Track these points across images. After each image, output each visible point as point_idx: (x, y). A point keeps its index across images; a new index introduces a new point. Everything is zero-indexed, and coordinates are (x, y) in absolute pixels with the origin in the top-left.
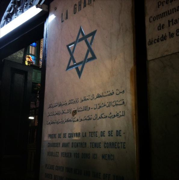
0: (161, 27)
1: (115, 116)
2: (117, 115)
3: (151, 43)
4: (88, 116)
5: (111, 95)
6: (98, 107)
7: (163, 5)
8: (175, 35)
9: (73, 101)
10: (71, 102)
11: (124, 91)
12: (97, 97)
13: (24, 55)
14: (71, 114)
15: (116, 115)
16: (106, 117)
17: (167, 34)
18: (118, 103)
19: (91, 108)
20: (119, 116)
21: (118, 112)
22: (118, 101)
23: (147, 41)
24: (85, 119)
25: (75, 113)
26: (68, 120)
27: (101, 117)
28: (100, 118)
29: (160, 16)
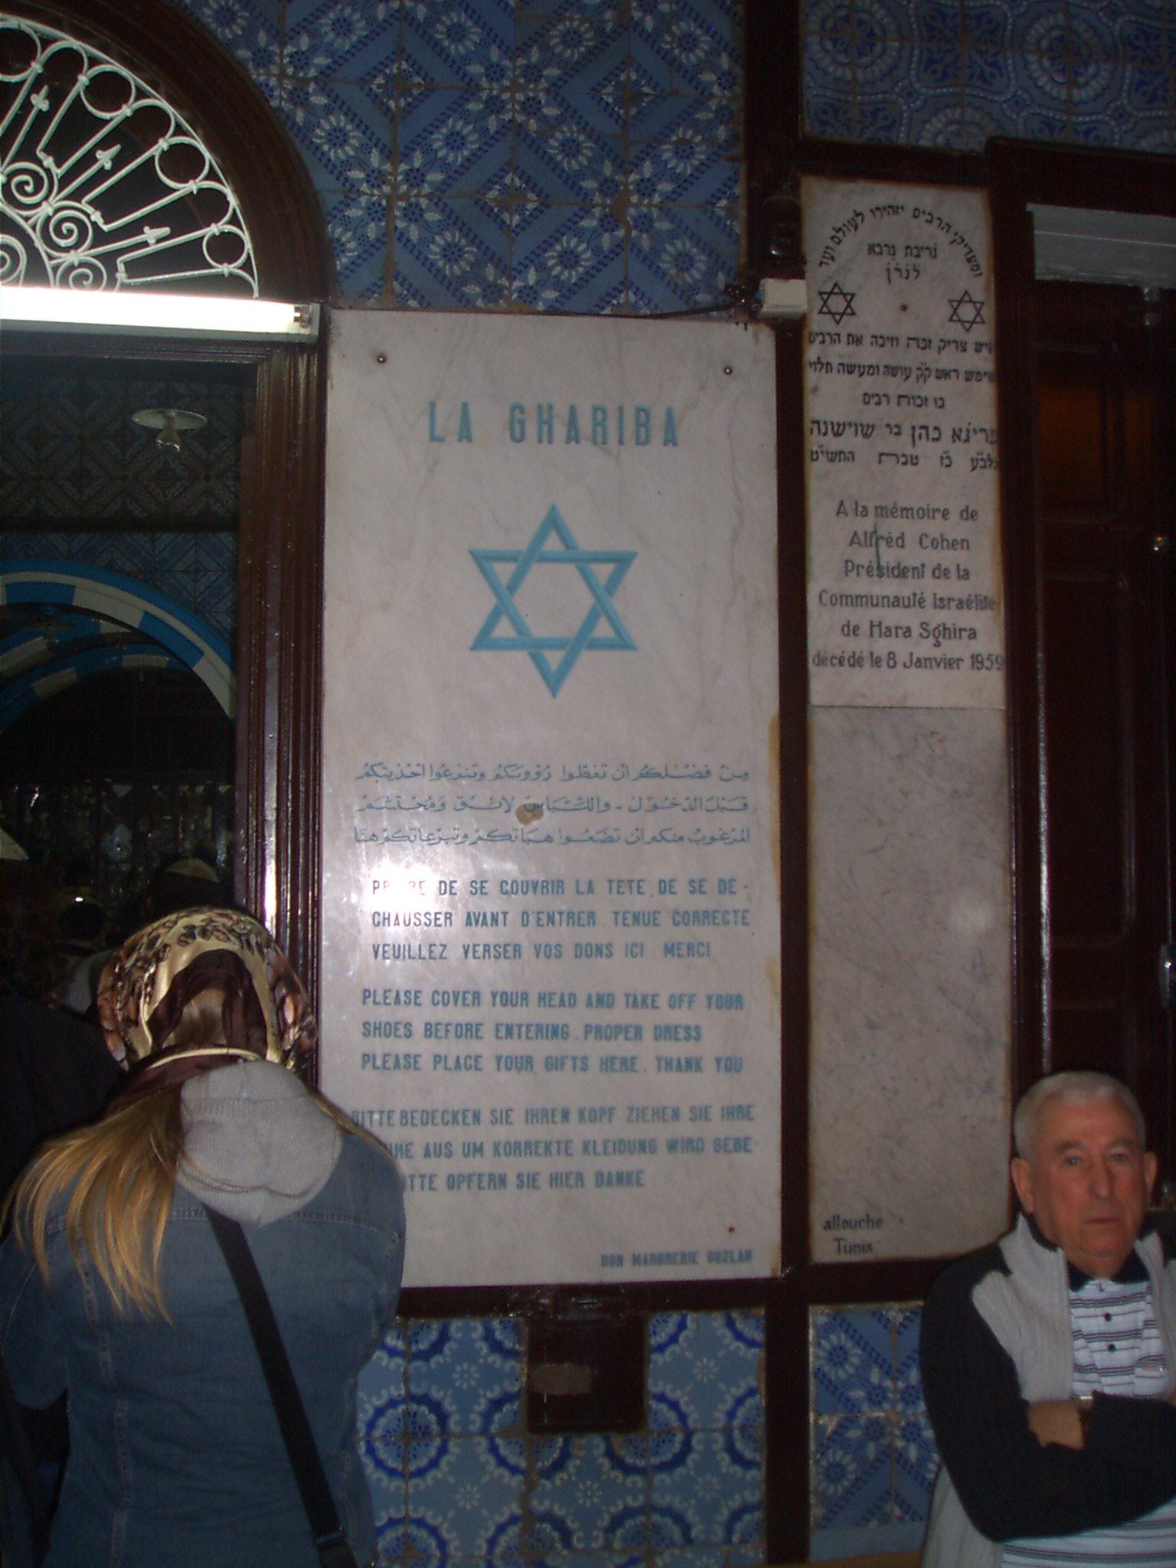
8: (884, 663)
9: (522, 771)
11: (746, 774)
12: (641, 776)
17: (866, 655)
28: (654, 839)
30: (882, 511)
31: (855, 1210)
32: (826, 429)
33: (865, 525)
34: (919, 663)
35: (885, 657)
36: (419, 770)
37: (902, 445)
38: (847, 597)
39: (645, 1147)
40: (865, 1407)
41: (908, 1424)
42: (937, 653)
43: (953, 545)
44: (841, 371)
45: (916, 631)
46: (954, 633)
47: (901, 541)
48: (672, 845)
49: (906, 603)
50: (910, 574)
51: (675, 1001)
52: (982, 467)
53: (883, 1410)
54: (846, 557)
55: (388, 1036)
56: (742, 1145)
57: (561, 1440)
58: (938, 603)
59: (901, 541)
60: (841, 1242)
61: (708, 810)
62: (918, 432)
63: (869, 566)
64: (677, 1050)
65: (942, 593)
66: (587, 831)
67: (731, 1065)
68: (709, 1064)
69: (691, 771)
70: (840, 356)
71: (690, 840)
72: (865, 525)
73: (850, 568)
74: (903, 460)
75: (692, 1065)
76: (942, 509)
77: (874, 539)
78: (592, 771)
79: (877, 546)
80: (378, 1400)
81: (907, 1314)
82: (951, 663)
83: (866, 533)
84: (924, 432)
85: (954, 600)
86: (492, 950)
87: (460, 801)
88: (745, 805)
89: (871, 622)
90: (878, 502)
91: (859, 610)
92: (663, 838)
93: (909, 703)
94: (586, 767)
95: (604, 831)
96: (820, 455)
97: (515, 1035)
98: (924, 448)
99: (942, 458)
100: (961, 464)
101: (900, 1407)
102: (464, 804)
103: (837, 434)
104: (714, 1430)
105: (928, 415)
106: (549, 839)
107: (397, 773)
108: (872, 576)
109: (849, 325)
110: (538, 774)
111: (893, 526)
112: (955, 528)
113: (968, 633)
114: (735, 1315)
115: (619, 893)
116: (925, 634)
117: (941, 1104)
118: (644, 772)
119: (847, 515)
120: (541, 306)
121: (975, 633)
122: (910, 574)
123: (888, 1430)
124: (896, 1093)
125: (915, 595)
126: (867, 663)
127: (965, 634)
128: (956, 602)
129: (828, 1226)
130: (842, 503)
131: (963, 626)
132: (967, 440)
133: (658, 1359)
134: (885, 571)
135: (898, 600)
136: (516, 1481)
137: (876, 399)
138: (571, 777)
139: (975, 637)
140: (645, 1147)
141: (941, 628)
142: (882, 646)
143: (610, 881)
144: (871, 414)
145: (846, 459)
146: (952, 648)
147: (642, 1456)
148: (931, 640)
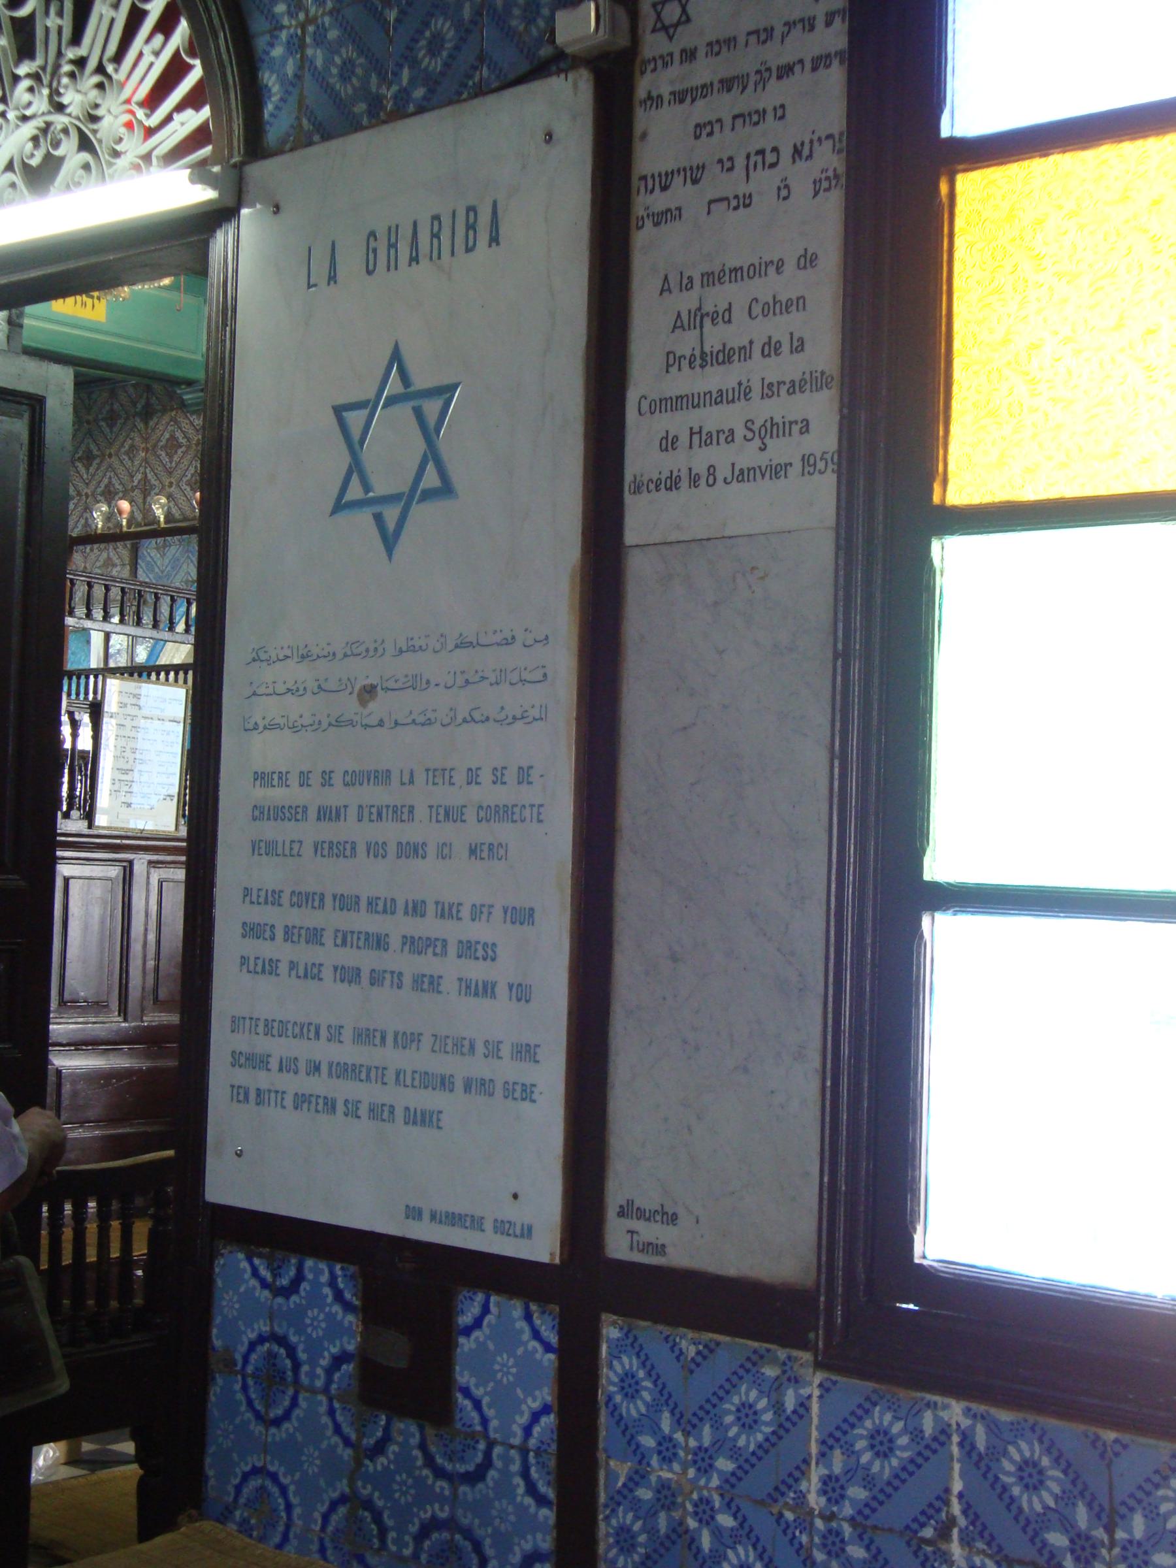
6: (460, 681)
7: (680, 369)
8: (703, 482)
9: (362, 649)
11: (547, 638)
12: (457, 646)
17: (684, 474)
22: (528, 670)
23: (628, 478)
24: (409, 720)
25: (368, 693)
28: (465, 721)
30: (710, 279)
31: (649, 1200)
32: (654, 185)
33: (686, 302)
34: (742, 475)
35: (704, 474)
36: (289, 653)
37: (734, 184)
38: (666, 399)
39: (445, 1083)
40: (655, 1461)
41: (701, 1499)
42: (762, 460)
43: (787, 307)
44: (672, 102)
45: (740, 432)
46: (773, 429)
47: (726, 315)
48: (480, 725)
49: (730, 397)
50: (736, 357)
51: (477, 912)
52: (825, 190)
53: (671, 1470)
54: (667, 350)
55: (258, 938)
56: (527, 1093)
57: (384, 1417)
58: (766, 391)
59: (726, 315)
60: (635, 1236)
61: (511, 684)
62: (753, 159)
63: (693, 355)
64: (477, 971)
65: (772, 378)
66: (411, 713)
67: (521, 993)
68: (502, 990)
69: (498, 638)
70: (672, 82)
71: (495, 721)
72: (686, 302)
73: (671, 361)
74: (734, 203)
75: (487, 990)
76: (776, 260)
77: (698, 318)
78: (417, 643)
79: (701, 327)
80: (393, 1538)
81: (701, 1347)
82: (778, 471)
83: (690, 312)
84: (765, 158)
85: (784, 383)
86: (335, 847)
87: (316, 684)
88: (545, 675)
89: (691, 429)
90: (706, 268)
91: (679, 415)
92: (473, 720)
93: (727, 533)
94: (412, 639)
95: (424, 713)
96: (646, 220)
97: (349, 944)
98: (764, 181)
99: (779, 189)
100: (801, 188)
101: (691, 1472)
102: (319, 687)
103: (664, 188)
104: (512, 1447)
105: (769, 134)
106: (381, 724)
107: (274, 658)
108: (693, 368)
109: (685, 38)
110: (376, 650)
111: (717, 297)
112: (786, 285)
113: (800, 425)
114: (533, 1307)
115: (434, 784)
116: (750, 435)
117: (746, 1070)
118: (459, 642)
119: (670, 292)
120: (411, 108)
121: (807, 425)
122: (736, 357)
123: (679, 1500)
124: (697, 1048)
125: (740, 384)
126: (684, 483)
127: (796, 429)
128: (787, 386)
129: (621, 1214)
130: (666, 278)
131: (792, 419)
132: (810, 156)
133: (466, 1344)
134: (709, 359)
135: (721, 395)
136: (347, 1454)
137: (708, 129)
138: (401, 651)
139: (807, 431)
140: (445, 1083)
141: (768, 425)
142: (701, 459)
143: (427, 770)
144: (705, 151)
145: (674, 218)
146: (781, 450)
147: (451, 1460)
148: (757, 442)
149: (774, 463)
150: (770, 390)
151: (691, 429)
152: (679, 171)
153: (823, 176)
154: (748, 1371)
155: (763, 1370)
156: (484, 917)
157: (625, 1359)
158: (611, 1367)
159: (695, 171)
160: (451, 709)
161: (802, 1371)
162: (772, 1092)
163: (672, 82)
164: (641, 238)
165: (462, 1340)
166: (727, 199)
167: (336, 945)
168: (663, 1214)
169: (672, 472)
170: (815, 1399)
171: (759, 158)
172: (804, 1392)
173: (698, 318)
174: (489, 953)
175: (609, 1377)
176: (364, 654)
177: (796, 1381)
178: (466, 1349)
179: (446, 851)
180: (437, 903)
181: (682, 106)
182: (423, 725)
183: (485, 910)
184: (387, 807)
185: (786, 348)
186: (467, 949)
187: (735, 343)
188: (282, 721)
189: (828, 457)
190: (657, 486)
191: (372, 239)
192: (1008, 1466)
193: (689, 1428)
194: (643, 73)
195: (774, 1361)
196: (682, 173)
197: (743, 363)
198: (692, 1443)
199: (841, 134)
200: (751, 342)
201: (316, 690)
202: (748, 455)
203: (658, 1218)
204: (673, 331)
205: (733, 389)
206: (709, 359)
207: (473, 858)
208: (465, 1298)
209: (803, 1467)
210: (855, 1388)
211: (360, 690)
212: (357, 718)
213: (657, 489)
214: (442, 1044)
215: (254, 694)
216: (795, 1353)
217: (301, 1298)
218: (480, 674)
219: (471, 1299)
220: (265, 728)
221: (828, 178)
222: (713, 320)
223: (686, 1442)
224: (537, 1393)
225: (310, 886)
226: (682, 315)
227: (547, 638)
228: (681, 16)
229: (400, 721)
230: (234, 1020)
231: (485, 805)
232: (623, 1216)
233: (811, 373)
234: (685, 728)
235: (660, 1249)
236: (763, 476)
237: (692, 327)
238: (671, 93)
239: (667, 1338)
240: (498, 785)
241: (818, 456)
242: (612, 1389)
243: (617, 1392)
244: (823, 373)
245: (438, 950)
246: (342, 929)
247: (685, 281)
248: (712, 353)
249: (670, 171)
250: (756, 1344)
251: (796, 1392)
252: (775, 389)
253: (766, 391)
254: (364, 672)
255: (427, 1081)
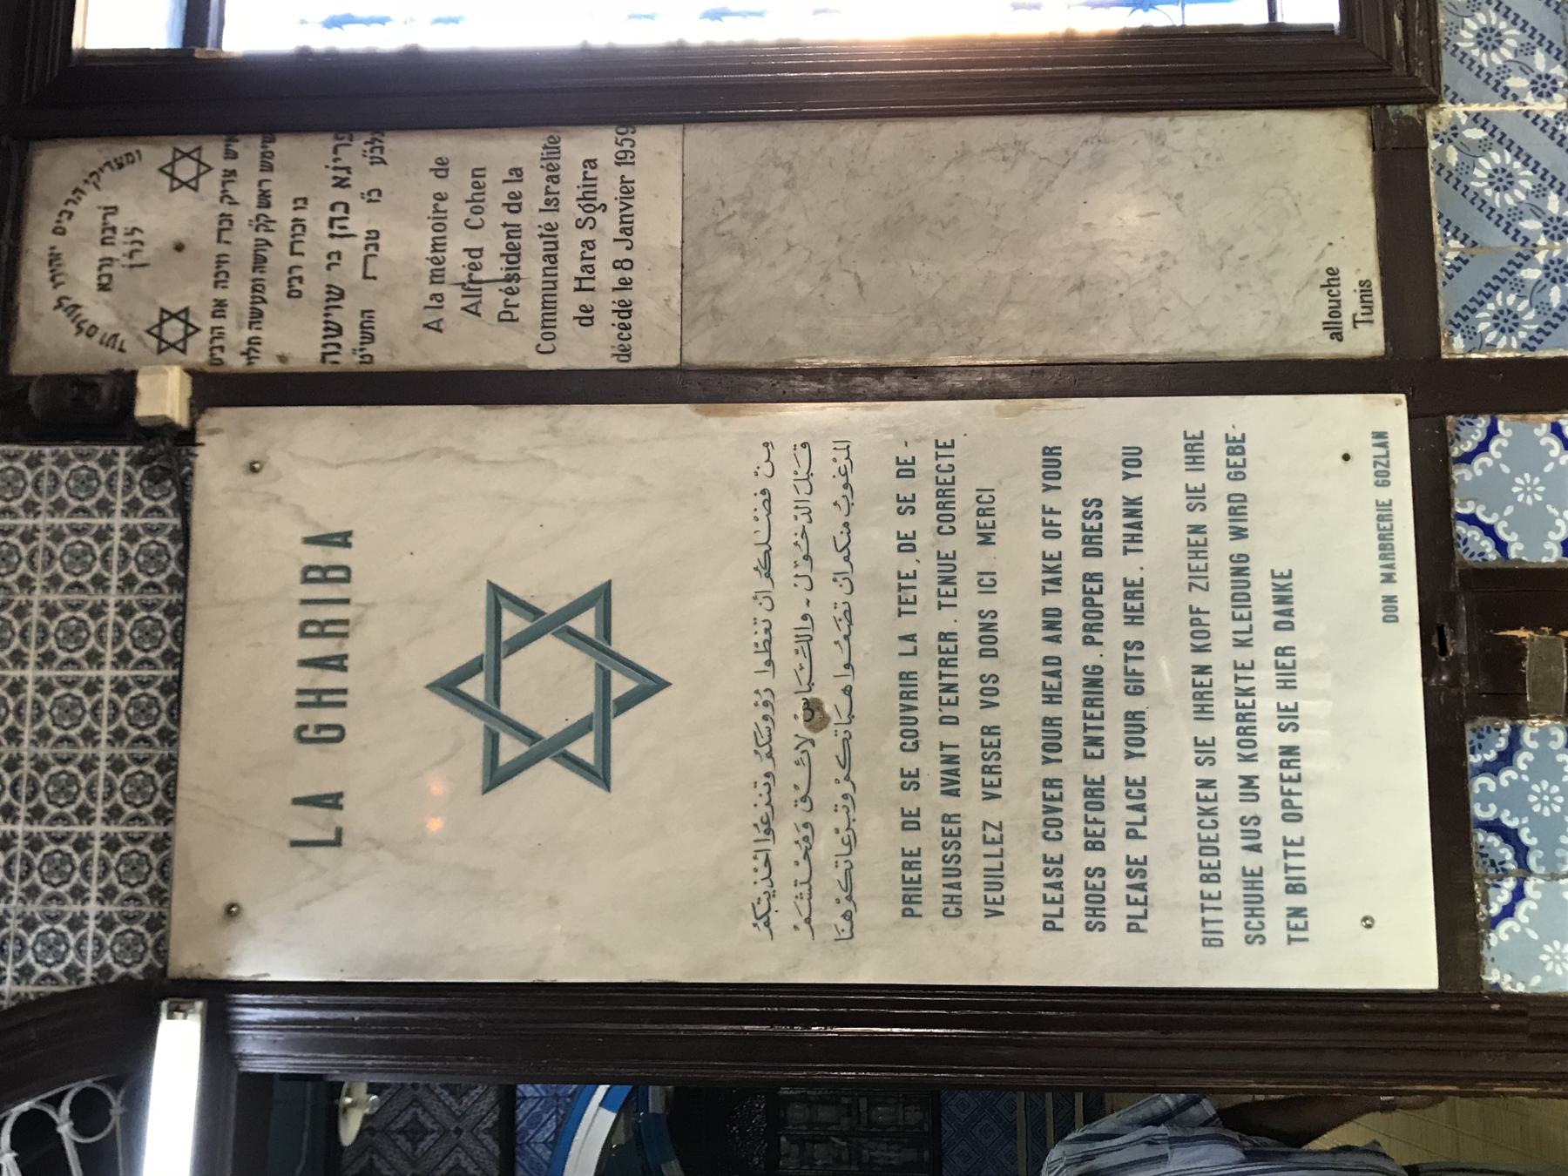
0: (586, 317)
1: (846, 485)
2: (768, 822)
3: (515, 249)
4: (837, 621)
5: (769, 501)
6: (804, 569)
7: (517, 306)
8: (627, 274)
9: (763, 725)
10: (764, 746)
11: (766, 444)
12: (768, 575)
13: (513, 1116)
14: (816, 736)
15: (843, 480)
16: (846, 525)
17: (617, 296)
18: (802, 474)
19: (805, 610)
20: (849, 466)
21: (836, 472)
22: (797, 469)
23: (613, 364)
24: (844, 644)
25: (813, 709)
26: (844, 885)
27: (845, 553)
28: (847, 559)
29: (438, 241)
34: (627, 230)
35: (620, 273)
36: (762, 856)
39: (1240, 568)
42: (614, 208)
43: (478, 187)
45: (586, 235)
52: (382, 152)
62: (336, 231)
64: (1114, 530)
67: (1132, 460)
70: (240, 327)
73: (508, 316)
74: (372, 250)
75: (1133, 509)
77: (471, 287)
78: (763, 636)
79: (480, 282)
82: (627, 190)
83: (464, 296)
89: (576, 290)
94: (756, 645)
96: (365, 352)
99: (370, 201)
106: (848, 691)
110: (766, 704)
114: (1455, 452)
116: (590, 223)
117: (1179, 196)
118: (763, 572)
122: (515, 241)
125: (541, 236)
129: (1337, 336)
130: (426, 326)
134: (512, 272)
138: (769, 662)
141: (583, 203)
142: (606, 276)
146: (608, 190)
148: (598, 215)
149: (619, 195)
150: (552, 203)
151: (576, 290)
152: (326, 315)
153: (369, 154)
154: (1459, 181)
155: (1454, 164)
156: (1056, 519)
157: (1482, 327)
158: (1492, 346)
159: (330, 333)
160: (835, 580)
161: (1445, 122)
162: (1196, 166)
163: (240, 327)
164: (384, 358)
165: (1513, 555)
166: (366, 259)
167: (1102, 757)
168: (1330, 285)
169: (614, 311)
170: (1468, 109)
171: (337, 223)
172: (1464, 120)
173: (471, 287)
174: (1092, 509)
175: (1506, 348)
176: (769, 724)
177: (1455, 128)
178: (1521, 547)
179: (987, 580)
180: (1045, 591)
181: (266, 313)
182: (850, 623)
183: (1049, 518)
184: (941, 675)
185: (515, 188)
186: (1092, 545)
187: (501, 243)
188: (843, 866)
189: (620, 138)
190: (626, 329)
191: (305, 734)
192: (1511, 299)
193: (1529, 245)
194: (221, 362)
195: (1442, 152)
196: (331, 311)
197: (523, 234)
198: (1542, 241)
199: (337, 138)
200: (505, 225)
201: (807, 806)
202: (609, 223)
203: (1334, 291)
204: (479, 315)
205: (545, 243)
206: (512, 272)
207: (993, 539)
208: (1466, 550)
209: (1532, 116)
210: (1449, 68)
211: (809, 728)
212: (841, 729)
213: (628, 328)
214: (1197, 579)
215: (808, 921)
216: (1430, 131)
217: (1520, 772)
218: (798, 538)
219: (1465, 542)
220: (849, 898)
221: (372, 151)
222: (477, 269)
223: (1544, 248)
224: (1543, 442)
225: (1035, 804)
226: (465, 305)
227: (766, 444)
228: (179, 341)
229: (846, 661)
230: (1207, 943)
231: (937, 524)
232: (1340, 334)
233: (543, 159)
234: (859, 285)
235: (1365, 286)
236: (630, 206)
237: (478, 293)
238: (250, 328)
239: (1450, 277)
240: (921, 780)
241: (619, 148)
242: (1515, 344)
243: (1516, 336)
244: (545, 147)
245: (1096, 587)
246: (1082, 747)
247: (434, 303)
248: (507, 269)
249: (324, 326)
250: (1432, 174)
251: (1464, 128)
252: (551, 197)
253: (552, 207)
254: (790, 710)
255: (1241, 598)
